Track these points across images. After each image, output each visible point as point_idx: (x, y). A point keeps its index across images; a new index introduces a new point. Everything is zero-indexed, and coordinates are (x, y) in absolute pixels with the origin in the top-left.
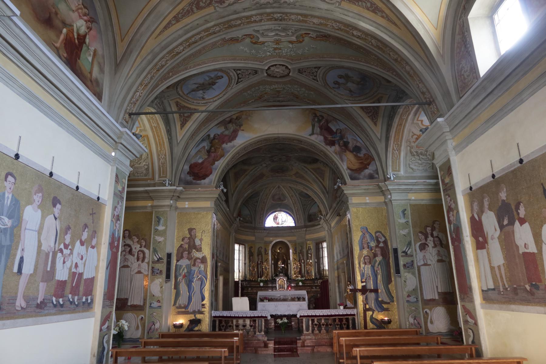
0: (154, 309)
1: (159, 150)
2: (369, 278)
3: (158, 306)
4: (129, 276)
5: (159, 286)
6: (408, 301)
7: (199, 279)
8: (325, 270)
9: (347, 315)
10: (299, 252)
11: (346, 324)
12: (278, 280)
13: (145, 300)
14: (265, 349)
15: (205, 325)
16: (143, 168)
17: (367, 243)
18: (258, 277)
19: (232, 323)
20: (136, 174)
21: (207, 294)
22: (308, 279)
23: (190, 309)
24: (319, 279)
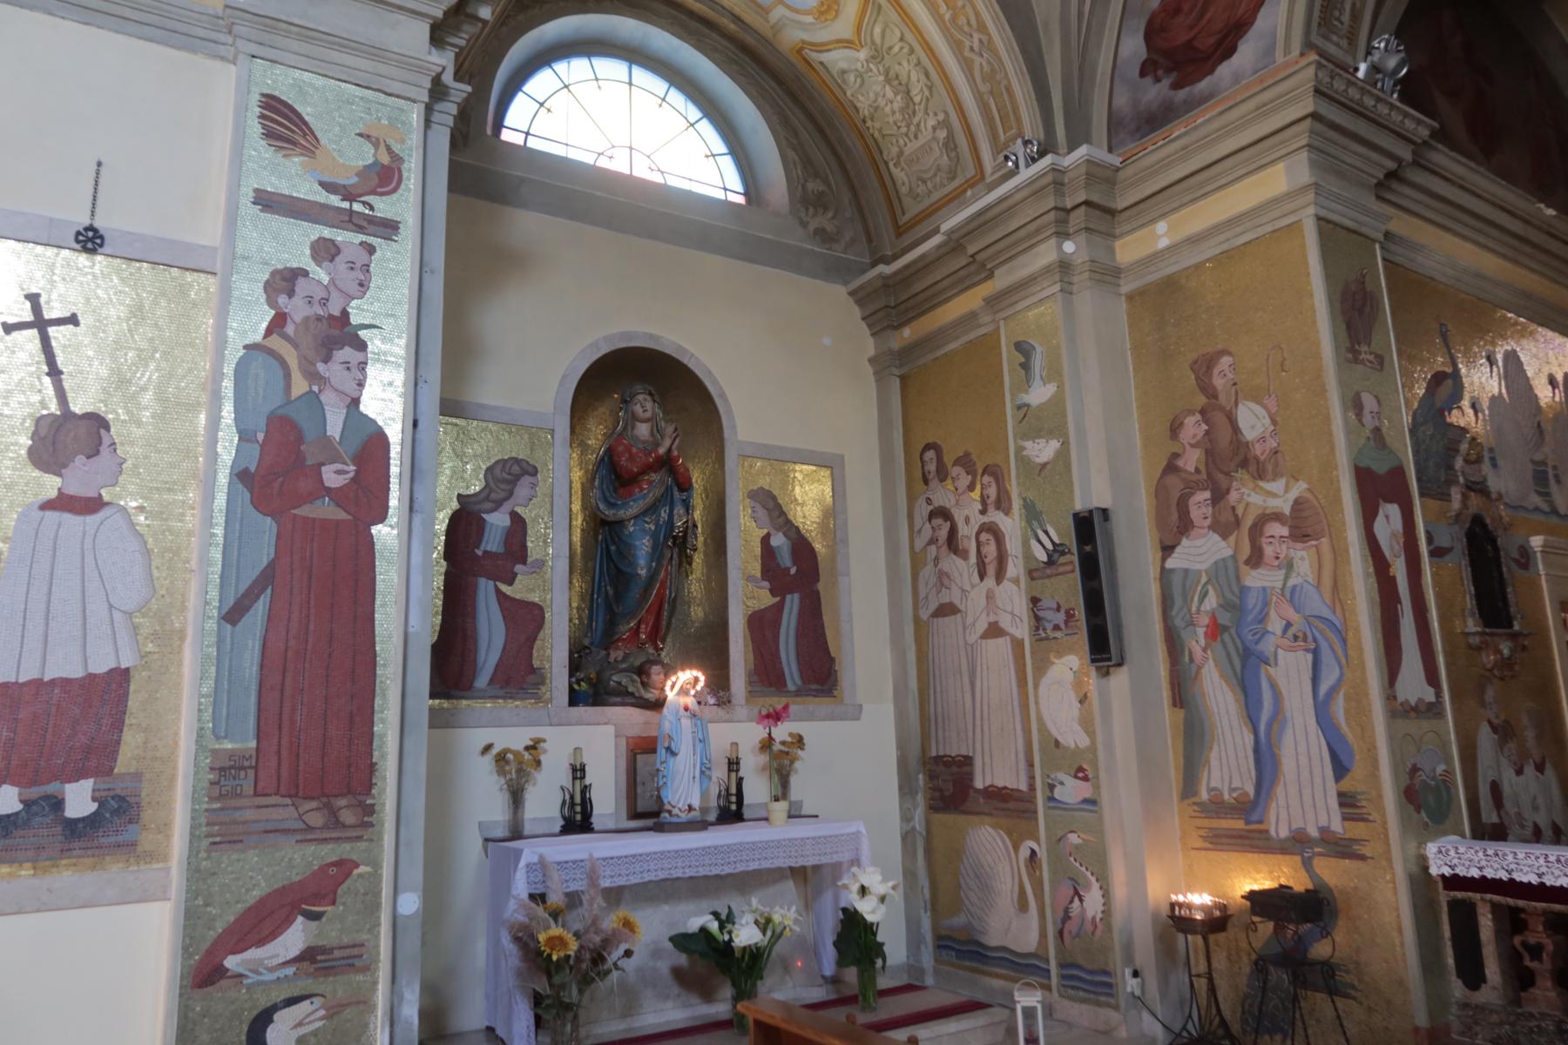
1: (947, 16)
3: (1085, 801)
4: (963, 653)
16: (935, 146)
20: (921, 189)
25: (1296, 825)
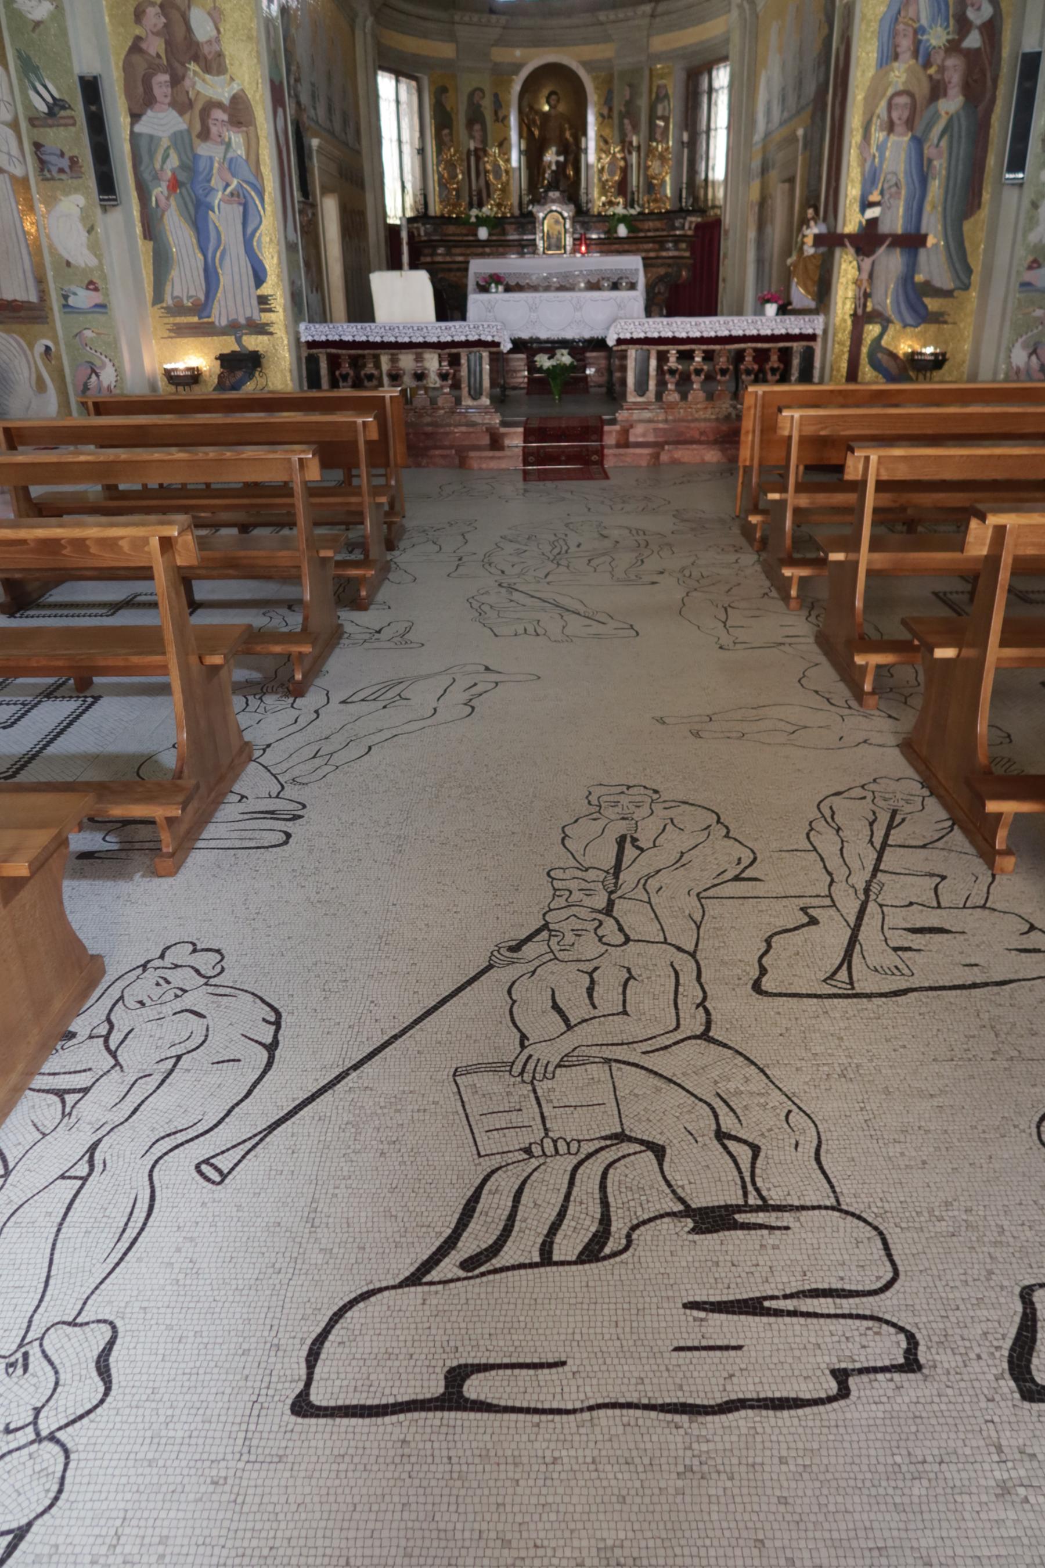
0: (81, 318)
2: (894, 189)
3: (97, 306)
5: (80, 226)
6: (1026, 285)
7: (232, 194)
8: (713, 182)
9: (788, 337)
10: (623, 109)
11: (778, 369)
12: (541, 215)
13: (40, 281)
14: (491, 454)
15: (279, 375)
17: (916, 32)
18: (471, 206)
19: (378, 365)
21: (272, 258)
22: (651, 213)
23: (219, 316)
24: (689, 213)
25: (232, 317)
